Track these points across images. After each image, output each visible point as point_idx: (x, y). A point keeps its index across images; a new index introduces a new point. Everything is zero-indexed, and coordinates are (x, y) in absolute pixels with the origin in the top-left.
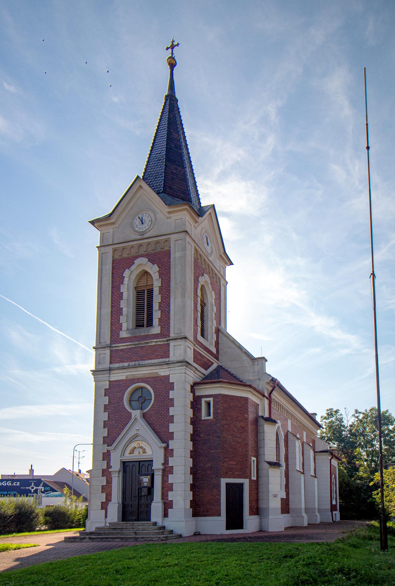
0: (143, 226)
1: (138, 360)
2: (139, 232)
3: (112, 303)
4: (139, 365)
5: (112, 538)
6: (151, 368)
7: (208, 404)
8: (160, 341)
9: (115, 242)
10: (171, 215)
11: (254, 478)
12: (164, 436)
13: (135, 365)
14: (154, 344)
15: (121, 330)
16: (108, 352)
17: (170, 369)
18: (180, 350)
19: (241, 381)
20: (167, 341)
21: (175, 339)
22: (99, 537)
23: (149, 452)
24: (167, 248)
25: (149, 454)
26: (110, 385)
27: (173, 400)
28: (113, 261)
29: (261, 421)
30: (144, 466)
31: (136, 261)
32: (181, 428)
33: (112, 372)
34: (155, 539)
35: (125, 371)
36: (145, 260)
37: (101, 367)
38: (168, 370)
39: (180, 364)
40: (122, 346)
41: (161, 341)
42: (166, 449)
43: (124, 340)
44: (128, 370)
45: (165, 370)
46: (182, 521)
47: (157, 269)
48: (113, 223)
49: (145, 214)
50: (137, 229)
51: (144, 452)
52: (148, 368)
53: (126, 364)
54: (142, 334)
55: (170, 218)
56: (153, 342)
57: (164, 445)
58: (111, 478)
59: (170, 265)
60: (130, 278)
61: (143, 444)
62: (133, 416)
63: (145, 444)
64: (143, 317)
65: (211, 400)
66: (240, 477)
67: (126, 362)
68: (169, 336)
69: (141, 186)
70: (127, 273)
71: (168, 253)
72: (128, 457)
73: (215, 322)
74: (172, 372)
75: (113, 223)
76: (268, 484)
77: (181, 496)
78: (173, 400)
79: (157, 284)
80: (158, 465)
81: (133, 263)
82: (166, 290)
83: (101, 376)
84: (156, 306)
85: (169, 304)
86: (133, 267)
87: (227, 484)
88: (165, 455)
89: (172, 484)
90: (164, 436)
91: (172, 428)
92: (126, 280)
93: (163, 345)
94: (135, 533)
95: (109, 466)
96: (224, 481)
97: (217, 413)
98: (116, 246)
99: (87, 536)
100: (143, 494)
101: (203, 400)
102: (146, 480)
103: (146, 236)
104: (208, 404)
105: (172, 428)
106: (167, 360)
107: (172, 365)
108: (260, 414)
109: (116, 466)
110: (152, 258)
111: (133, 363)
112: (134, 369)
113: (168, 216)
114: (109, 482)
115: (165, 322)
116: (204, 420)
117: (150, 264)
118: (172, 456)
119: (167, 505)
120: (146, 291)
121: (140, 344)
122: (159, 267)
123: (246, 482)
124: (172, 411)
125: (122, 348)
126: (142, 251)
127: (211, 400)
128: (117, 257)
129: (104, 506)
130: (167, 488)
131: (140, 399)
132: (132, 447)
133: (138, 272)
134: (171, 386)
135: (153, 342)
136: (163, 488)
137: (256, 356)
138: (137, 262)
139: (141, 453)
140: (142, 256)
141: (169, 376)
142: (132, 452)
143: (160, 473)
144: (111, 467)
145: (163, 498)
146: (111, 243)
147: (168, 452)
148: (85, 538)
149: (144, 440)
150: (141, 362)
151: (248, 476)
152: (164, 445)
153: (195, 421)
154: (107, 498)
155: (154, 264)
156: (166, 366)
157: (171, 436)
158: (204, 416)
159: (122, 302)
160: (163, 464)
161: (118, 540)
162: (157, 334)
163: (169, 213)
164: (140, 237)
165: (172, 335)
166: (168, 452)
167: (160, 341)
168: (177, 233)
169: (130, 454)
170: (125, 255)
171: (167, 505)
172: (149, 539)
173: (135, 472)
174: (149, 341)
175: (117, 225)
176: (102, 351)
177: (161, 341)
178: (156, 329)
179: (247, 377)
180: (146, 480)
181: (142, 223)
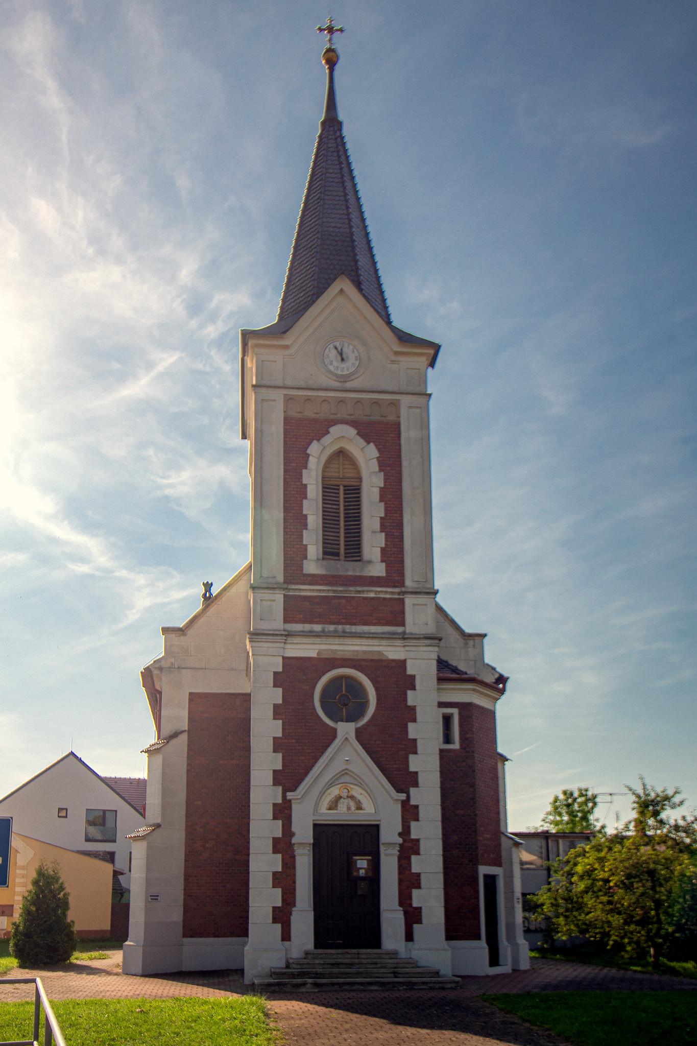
0: (348, 364)
1: (342, 624)
2: (337, 376)
3: (285, 502)
4: (344, 632)
5: (361, 984)
6: (371, 642)
8: (386, 592)
9: (289, 382)
10: (401, 358)
12: (403, 780)
13: (336, 631)
14: (372, 595)
15: (306, 558)
16: (279, 597)
17: (407, 648)
20: (399, 594)
21: (416, 593)
22: (335, 980)
23: (369, 808)
24: (392, 418)
25: (368, 812)
28: (285, 419)
30: (366, 837)
31: (332, 430)
33: (290, 640)
34: (449, 986)
35: (318, 640)
36: (352, 432)
37: (265, 626)
38: (403, 649)
39: (432, 641)
40: (307, 590)
41: (386, 593)
42: (405, 804)
43: (314, 580)
44: (324, 640)
45: (397, 649)
46: (444, 950)
47: (376, 454)
48: (287, 347)
49: (346, 344)
50: (332, 368)
51: (359, 807)
52: (366, 642)
53: (318, 628)
54: (350, 573)
55: (397, 362)
56: (372, 593)
57: (403, 796)
58: (294, 857)
59: (400, 450)
60: (317, 454)
61: (357, 792)
63: (360, 790)
64: (343, 539)
65: (455, 711)
67: (317, 623)
68: (402, 584)
69: (342, 291)
70: (314, 449)
71: (396, 428)
72: (327, 816)
74: (412, 655)
75: (287, 347)
80: (390, 834)
81: (327, 432)
83: (267, 645)
85: (402, 524)
86: (327, 440)
89: (418, 875)
90: (403, 780)
92: (312, 462)
93: (391, 599)
94: (394, 973)
95: (288, 832)
97: (467, 739)
98: (293, 392)
99: (310, 980)
100: (359, 892)
102: (362, 863)
103: (349, 385)
106: (400, 629)
107: (413, 642)
109: (303, 834)
111: (331, 628)
112: (337, 641)
113: (393, 358)
117: (361, 442)
119: (413, 916)
120: (342, 488)
121: (346, 591)
122: (379, 450)
125: (308, 594)
127: (455, 711)
128: (292, 414)
132: (333, 795)
133: (332, 451)
134: (410, 683)
135: (372, 593)
137: (468, 630)
138: (336, 430)
139: (353, 808)
141: (405, 661)
142: (333, 805)
143: (395, 851)
144: (292, 835)
146: (279, 382)
147: (410, 812)
148: (304, 984)
149: (361, 784)
150: (348, 628)
152: (403, 796)
155: (368, 443)
156: (399, 643)
159: (305, 502)
160: (400, 835)
161: (375, 988)
162: (379, 578)
163: (397, 353)
164: (337, 385)
165: (409, 583)
166: (410, 812)
167: (386, 592)
168: (407, 394)
169: (330, 809)
170: (310, 413)
172: (437, 986)
174: (365, 588)
175: (292, 351)
176: (266, 595)
177: (386, 593)
180: (362, 863)
181: (343, 360)
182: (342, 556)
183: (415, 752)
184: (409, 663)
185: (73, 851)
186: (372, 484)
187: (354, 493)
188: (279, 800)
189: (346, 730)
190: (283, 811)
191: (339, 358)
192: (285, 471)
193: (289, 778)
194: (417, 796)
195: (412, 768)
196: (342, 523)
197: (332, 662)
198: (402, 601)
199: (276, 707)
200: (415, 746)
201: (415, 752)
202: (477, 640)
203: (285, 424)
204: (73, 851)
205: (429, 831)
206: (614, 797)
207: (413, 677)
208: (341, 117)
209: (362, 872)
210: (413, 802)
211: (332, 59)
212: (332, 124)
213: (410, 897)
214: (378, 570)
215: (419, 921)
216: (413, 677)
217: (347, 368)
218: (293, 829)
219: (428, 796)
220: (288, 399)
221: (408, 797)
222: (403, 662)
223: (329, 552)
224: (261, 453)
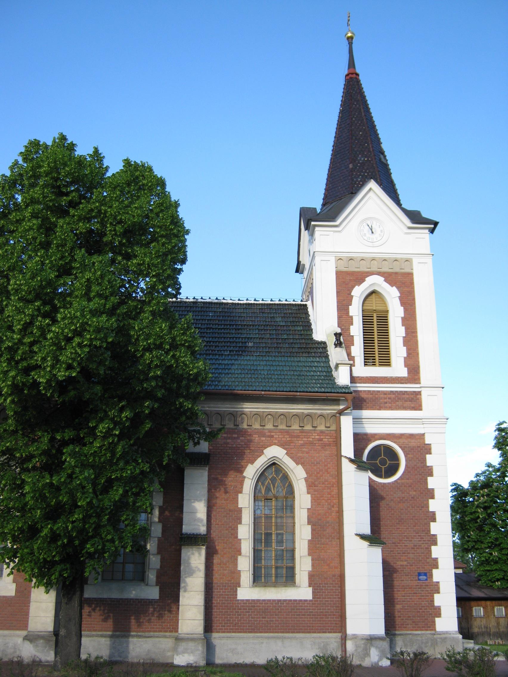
24: (407, 270)
50: (365, 238)
60: (358, 293)
181: (372, 233)
182: (377, 363)
183: (437, 568)
184: (426, 436)
185: (351, 63)
186: (396, 313)
187: (383, 320)
191: (371, 232)
200: (430, 449)
201: (437, 568)
204: (351, 63)
208: (358, 71)
214: (403, 372)
216: (434, 513)
224: (269, 638)
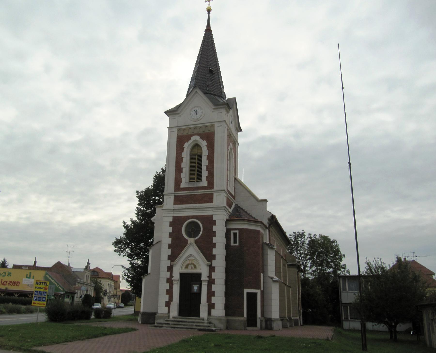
0: (197, 115)
3: (176, 164)
7: (235, 234)
11: (262, 289)
12: (210, 257)
18: (220, 200)
19: (254, 218)
24: (212, 131)
26: (173, 219)
27: (215, 232)
29: (266, 247)
30: (197, 278)
31: (192, 138)
32: (219, 252)
47: (206, 144)
60: (187, 146)
62: (189, 242)
64: (195, 173)
66: (255, 289)
70: (186, 145)
71: (213, 134)
73: (233, 153)
76: (271, 294)
77: (219, 301)
78: (215, 232)
79: (205, 152)
80: (204, 277)
81: (190, 139)
82: (211, 158)
84: (204, 168)
87: (248, 293)
88: (210, 271)
90: (210, 257)
91: (215, 228)
96: (246, 291)
101: (232, 232)
104: (235, 234)
105: (214, 251)
108: (264, 242)
109: (176, 276)
110: (203, 137)
114: (171, 287)
115: (210, 178)
116: (232, 246)
118: (214, 272)
119: (211, 306)
120: (197, 156)
122: (207, 142)
123: (258, 292)
124: (215, 228)
126: (196, 132)
127: (237, 232)
129: (168, 304)
130: (211, 294)
131: (193, 230)
134: (214, 223)
136: (208, 294)
140: (196, 135)
144: (173, 277)
145: (207, 302)
147: (212, 269)
151: (259, 288)
153: (228, 246)
154: (169, 299)
157: (214, 257)
158: (232, 244)
160: (208, 277)
162: (205, 187)
166: (212, 269)
170: (185, 134)
171: (211, 306)
173: (189, 280)
178: (204, 183)
179: (255, 214)
180: (196, 288)
182: (196, 180)
187: (200, 157)
188: (213, 261)
189: (191, 240)
190: (170, 269)
192: (176, 154)
193: (172, 258)
194: (214, 263)
195: (214, 253)
196: (196, 168)
197: (188, 217)
198: (212, 194)
199: (170, 233)
202: (264, 203)
203: (177, 138)
205: (220, 276)
206: (418, 257)
207: (215, 221)
208: (212, 28)
209: (195, 291)
210: (213, 266)
211: (209, 11)
212: (208, 32)
213: (211, 299)
215: (214, 308)
217: (198, 116)
218: (173, 275)
219: (220, 264)
220: (179, 130)
221: (212, 264)
222: (212, 216)
223: (191, 180)
